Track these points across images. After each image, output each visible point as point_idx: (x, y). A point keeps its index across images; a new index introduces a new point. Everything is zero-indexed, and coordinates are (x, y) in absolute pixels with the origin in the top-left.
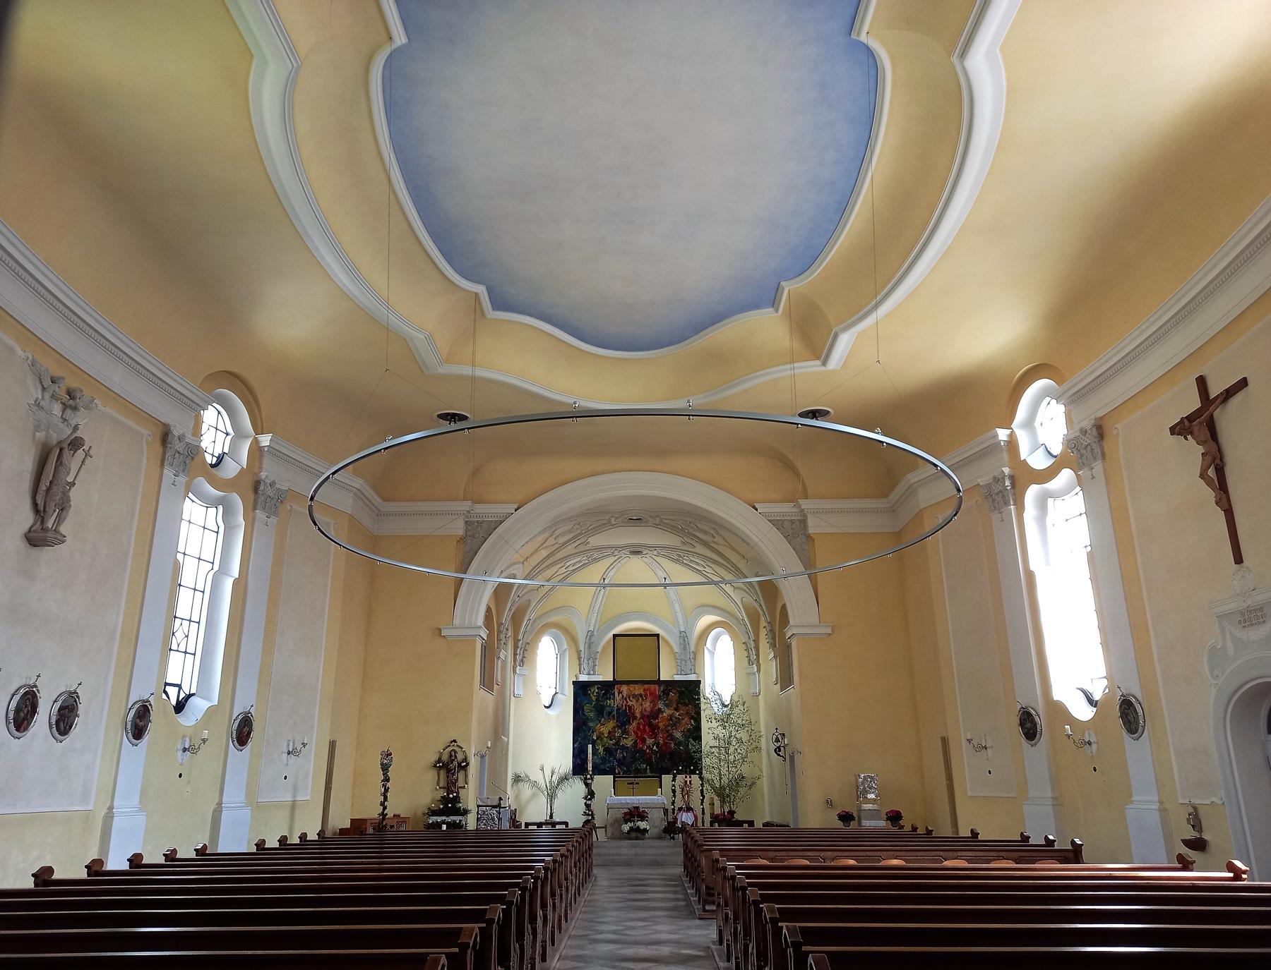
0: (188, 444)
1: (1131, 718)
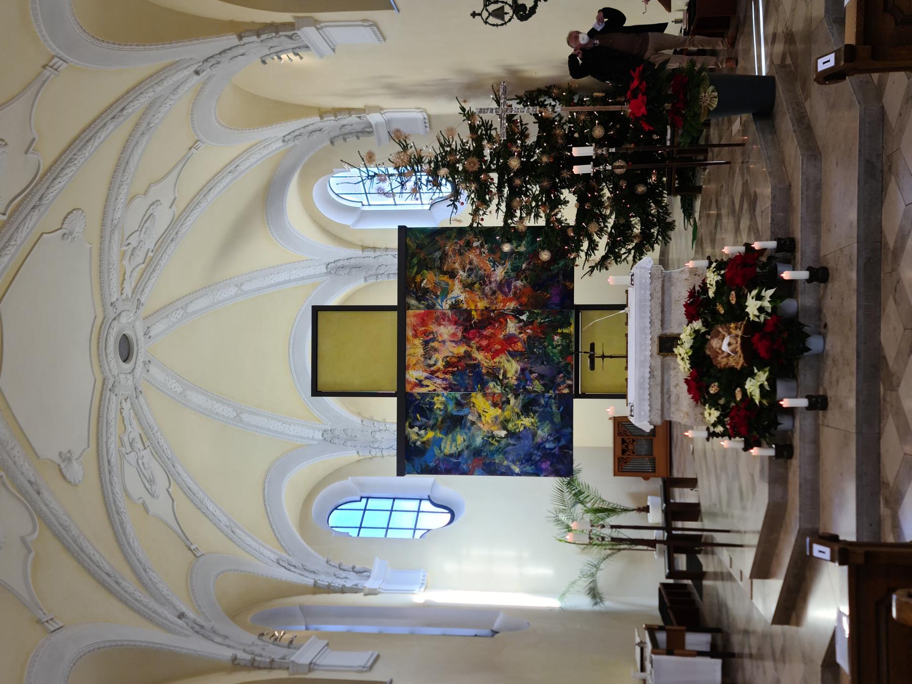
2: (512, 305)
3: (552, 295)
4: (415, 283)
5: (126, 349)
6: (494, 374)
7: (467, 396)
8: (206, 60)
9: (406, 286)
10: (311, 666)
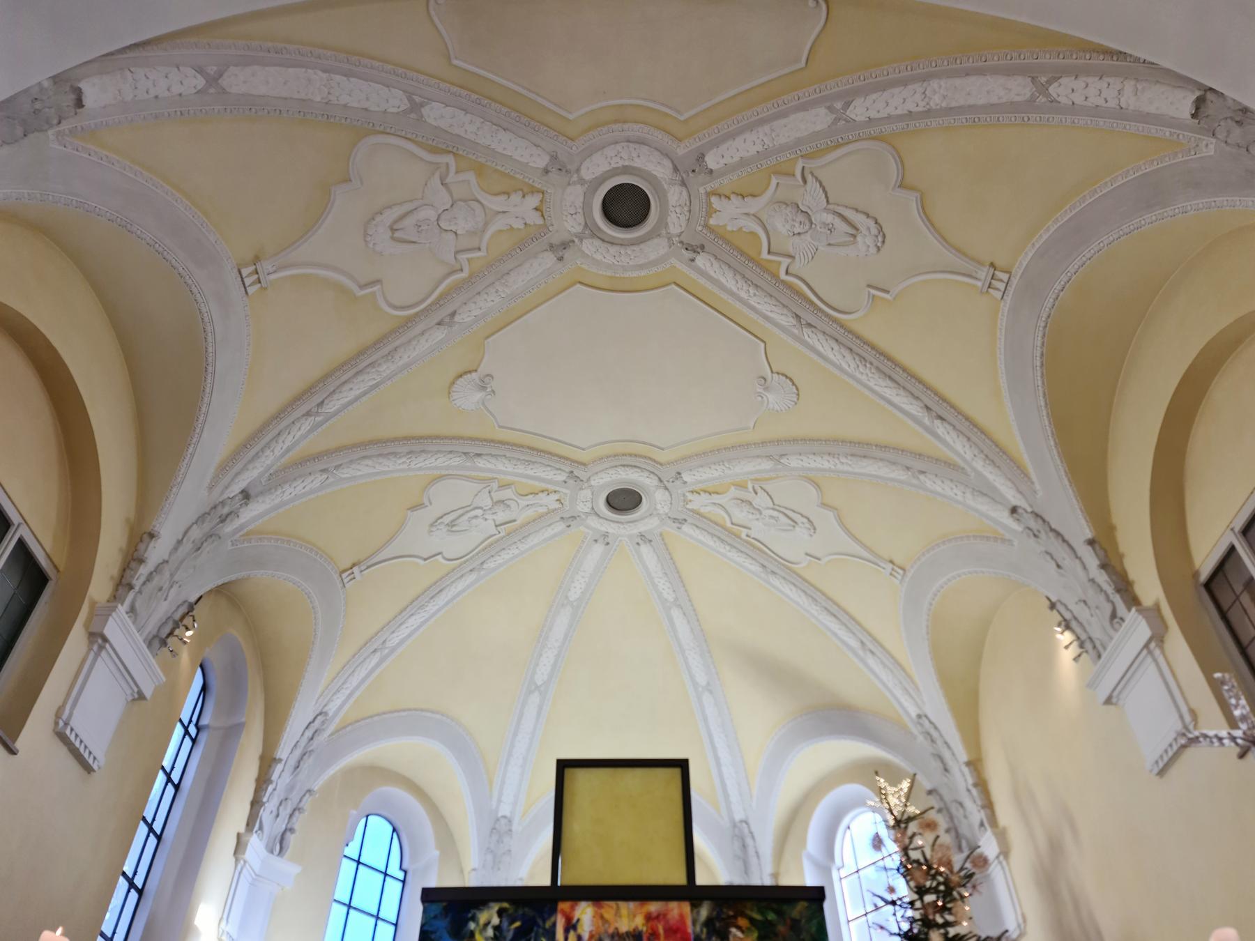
4: (735, 917)
5: (624, 501)
8: (1037, 515)
10: (97, 639)
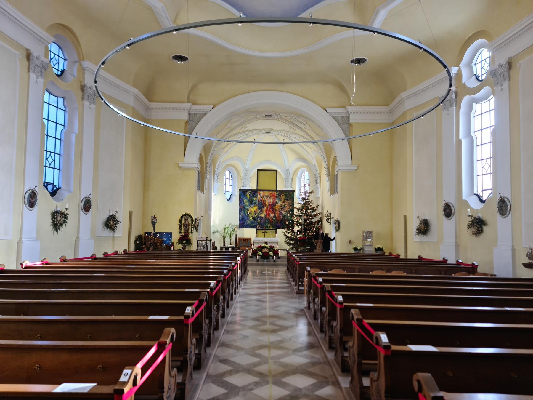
0: (42, 61)
1: (503, 208)
2: (277, 215)
3: (279, 224)
6: (261, 211)
7: (257, 205)
9: (281, 192)
